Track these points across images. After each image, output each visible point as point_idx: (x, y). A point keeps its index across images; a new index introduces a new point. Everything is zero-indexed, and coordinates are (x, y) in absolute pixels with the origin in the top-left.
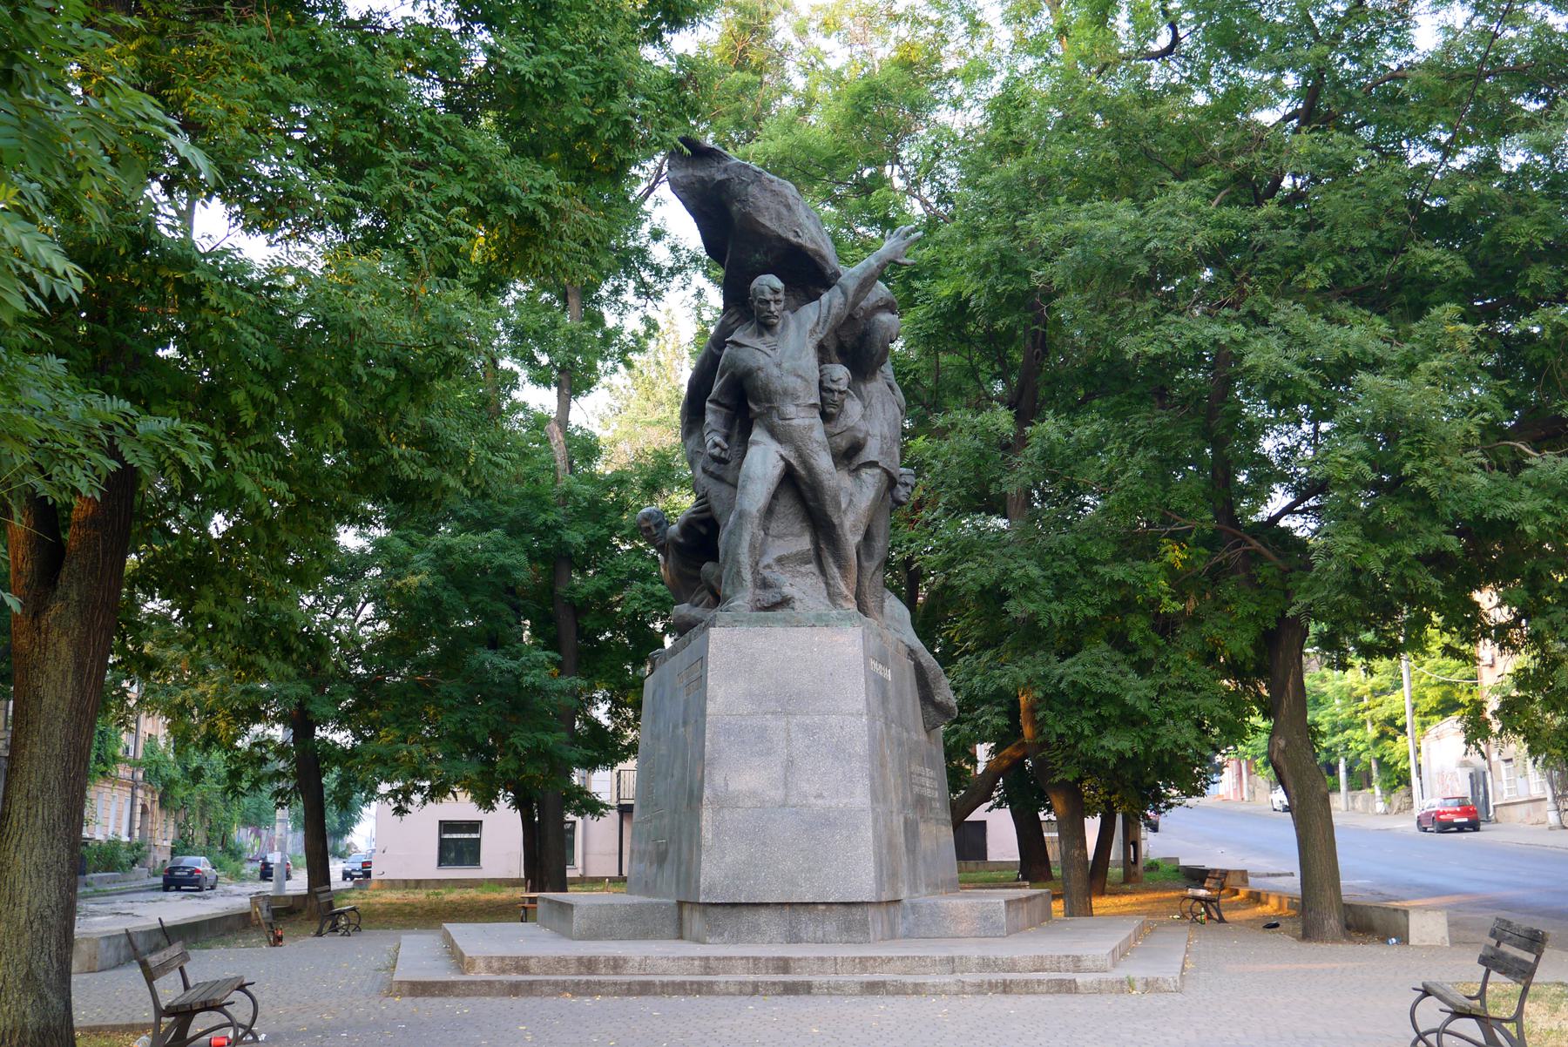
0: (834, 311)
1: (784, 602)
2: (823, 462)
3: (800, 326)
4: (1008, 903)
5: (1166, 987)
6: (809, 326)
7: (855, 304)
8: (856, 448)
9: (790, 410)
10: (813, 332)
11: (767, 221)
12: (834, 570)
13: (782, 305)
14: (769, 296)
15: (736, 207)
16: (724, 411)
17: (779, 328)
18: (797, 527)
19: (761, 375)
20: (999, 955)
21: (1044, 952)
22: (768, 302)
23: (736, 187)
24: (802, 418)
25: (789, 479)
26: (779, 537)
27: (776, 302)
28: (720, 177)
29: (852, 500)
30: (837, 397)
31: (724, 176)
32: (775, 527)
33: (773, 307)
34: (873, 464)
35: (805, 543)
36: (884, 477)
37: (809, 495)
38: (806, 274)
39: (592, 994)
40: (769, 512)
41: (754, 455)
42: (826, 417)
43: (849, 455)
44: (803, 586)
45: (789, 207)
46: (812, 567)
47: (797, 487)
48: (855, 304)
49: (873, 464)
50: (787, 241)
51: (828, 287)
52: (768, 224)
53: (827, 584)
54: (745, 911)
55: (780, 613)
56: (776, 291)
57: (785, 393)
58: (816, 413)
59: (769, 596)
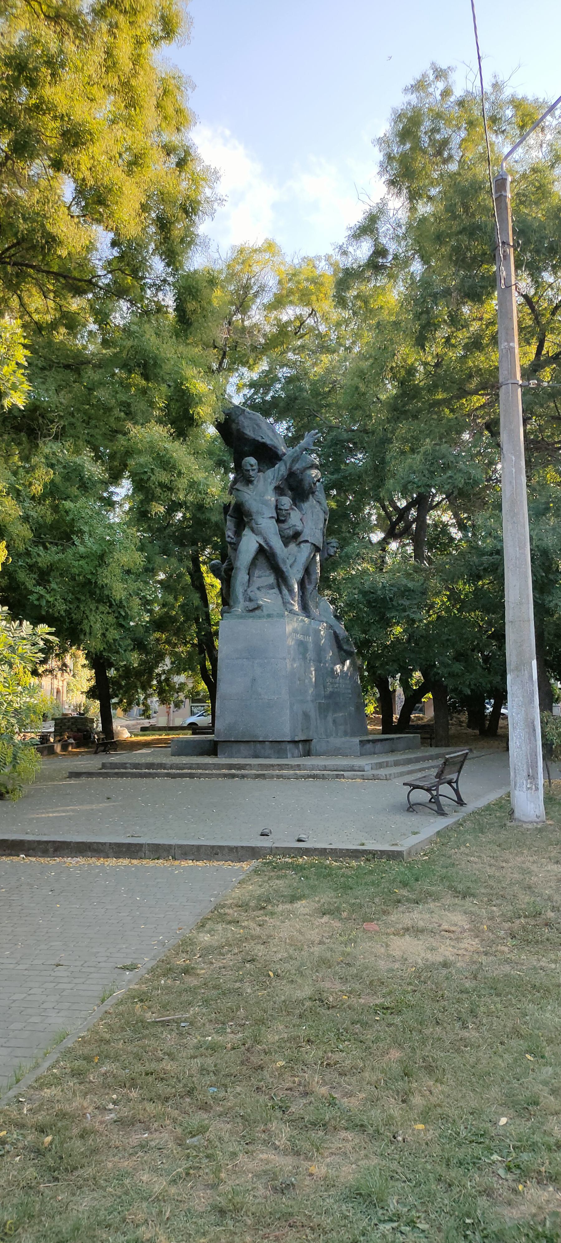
0: (281, 473)
1: (259, 607)
2: (277, 544)
3: (265, 480)
6: (269, 480)
7: (290, 469)
8: (297, 535)
11: (249, 432)
12: (285, 591)
14: (249, 468)
17: (255, 482)
18: (268, 572)
25: (261, 550)
26: (259, 577)
27: (253, 470)
29: (295, 559)
30: (284, 512)
32: (257, 573)
33: (251, 473)
34: (307, 541)
35: (271, 579)
38: (267, 455)
39: (122, 777)
40: (253, 563)
41: (244, 540)
42: (278, 521)
43: (293, 538)
44: (268, 599)
45: (258, 425)
46: (276, 590)
47: (265, 554)
49: (307, 541)
50: (258, 441)
52: (248, 433)
53: (283, 598)
54: (235, 745)
55: (257, 612)
56: (252, 466)
57: (258, 513)
58: (274, 521)
59: (251, 606)
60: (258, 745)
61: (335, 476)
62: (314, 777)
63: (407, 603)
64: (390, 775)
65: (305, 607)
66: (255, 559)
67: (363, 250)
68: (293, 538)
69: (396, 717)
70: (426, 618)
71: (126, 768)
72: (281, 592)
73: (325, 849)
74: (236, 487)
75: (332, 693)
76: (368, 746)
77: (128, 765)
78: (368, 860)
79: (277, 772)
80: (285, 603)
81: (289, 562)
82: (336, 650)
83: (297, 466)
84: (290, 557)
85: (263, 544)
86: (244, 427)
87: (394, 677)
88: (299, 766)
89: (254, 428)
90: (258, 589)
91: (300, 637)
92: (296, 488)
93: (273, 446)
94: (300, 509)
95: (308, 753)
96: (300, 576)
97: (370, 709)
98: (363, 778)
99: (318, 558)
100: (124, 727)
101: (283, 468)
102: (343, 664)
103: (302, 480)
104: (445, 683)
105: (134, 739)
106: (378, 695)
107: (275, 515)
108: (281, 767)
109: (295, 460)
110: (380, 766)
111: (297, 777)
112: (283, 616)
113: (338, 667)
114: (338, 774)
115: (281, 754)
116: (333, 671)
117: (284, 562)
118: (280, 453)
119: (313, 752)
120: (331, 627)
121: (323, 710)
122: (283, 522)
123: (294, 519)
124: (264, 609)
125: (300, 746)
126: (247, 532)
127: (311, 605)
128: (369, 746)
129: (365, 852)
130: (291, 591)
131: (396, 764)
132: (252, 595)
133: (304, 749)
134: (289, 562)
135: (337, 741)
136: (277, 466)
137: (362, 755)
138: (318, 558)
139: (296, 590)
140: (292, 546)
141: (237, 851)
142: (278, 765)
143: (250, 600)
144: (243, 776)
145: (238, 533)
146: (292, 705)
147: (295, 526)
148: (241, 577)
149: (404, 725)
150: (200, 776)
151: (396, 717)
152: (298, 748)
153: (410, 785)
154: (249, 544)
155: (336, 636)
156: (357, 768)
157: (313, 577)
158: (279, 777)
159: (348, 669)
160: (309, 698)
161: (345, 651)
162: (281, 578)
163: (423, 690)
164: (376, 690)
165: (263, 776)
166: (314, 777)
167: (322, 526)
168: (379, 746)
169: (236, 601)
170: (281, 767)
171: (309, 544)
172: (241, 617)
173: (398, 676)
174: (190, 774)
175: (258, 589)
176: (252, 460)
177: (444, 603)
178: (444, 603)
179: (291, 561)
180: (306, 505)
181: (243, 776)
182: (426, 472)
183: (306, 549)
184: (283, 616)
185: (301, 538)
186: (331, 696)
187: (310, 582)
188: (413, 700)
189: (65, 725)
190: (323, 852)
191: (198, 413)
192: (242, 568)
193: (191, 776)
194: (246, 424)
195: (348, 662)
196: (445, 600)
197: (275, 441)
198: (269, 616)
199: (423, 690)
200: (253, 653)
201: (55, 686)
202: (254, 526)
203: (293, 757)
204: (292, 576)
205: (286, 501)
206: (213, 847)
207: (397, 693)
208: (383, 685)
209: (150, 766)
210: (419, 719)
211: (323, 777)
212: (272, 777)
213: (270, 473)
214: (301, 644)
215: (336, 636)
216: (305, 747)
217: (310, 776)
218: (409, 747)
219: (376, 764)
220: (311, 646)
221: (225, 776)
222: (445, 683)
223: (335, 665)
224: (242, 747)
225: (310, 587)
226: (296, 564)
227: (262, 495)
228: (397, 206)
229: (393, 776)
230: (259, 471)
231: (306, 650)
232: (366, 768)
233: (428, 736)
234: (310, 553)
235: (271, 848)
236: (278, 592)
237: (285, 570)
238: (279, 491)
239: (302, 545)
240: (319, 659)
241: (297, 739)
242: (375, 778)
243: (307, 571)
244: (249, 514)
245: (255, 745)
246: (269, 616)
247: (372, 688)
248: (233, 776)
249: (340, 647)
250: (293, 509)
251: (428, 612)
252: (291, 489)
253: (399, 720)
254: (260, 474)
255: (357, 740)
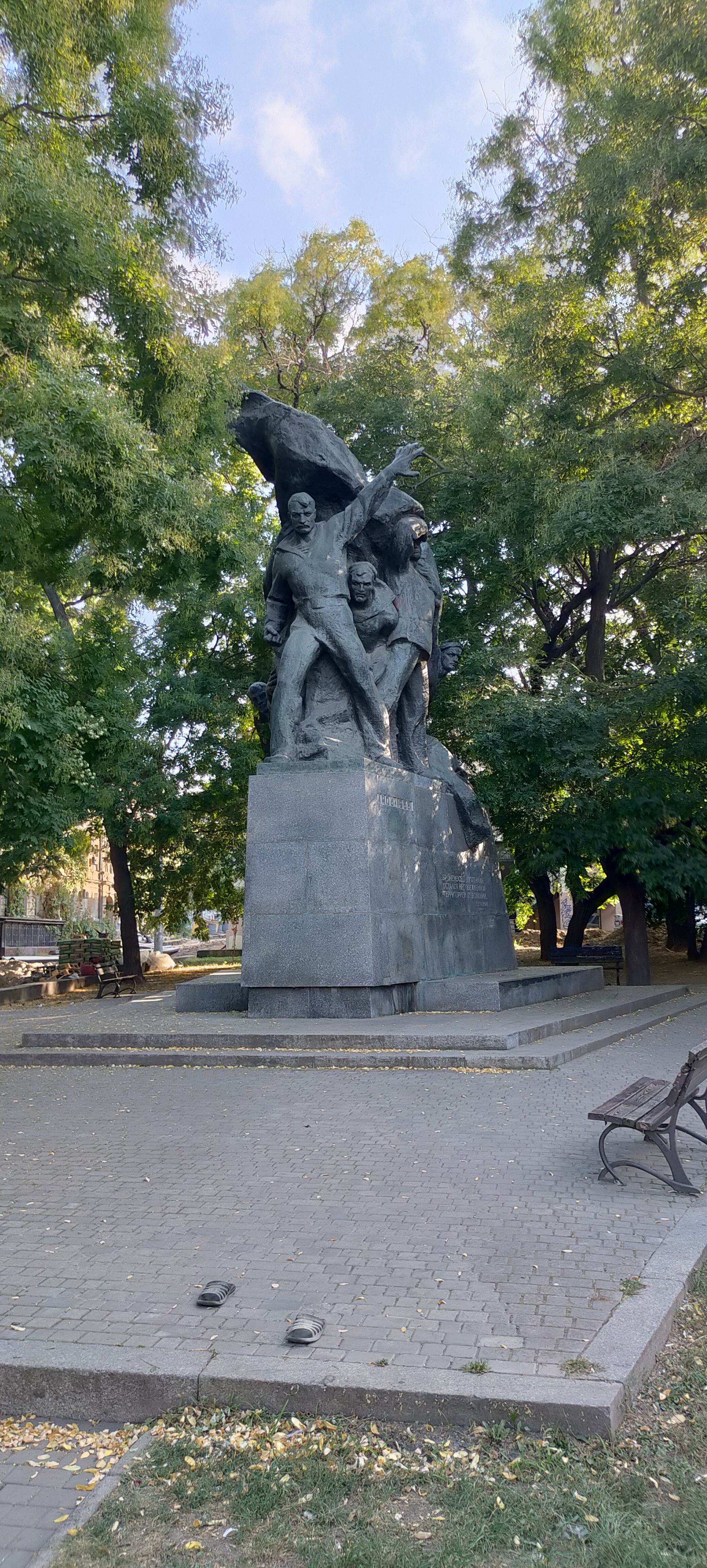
1: (320, 753)
3: (328, 532)
4: (505, 986)
5: (539, 1065)
6: (336, 532)
7: (372, 512)
8: (387, 628)
9: (321, 602)
10: (339, 536)
11: (298, 449)
12: (368, 726)
13: (313, 516)
15: (273, 440)
16: (280, 604)
17: (311, 536)
18: (336, 694)
19: (297, 573)
20: (419, 1034)
21: (434, 1034)
22: (299, 515)
23: (271, 423)
24: (333, 608)
27: (306, 514)
28: (260, 416)
29: (384, 672)
30: (362, 588)
31: (264, 415)
32: (318, 694)
33: (304, 519)
34: (404, 640)
35: (343, 705)
36: (414, 650)
37: (341, 667)
38: (333, 491)
43: (381, 634)
44: (338, 739)
45: (315, 437)
46: (351, 724)
47: (329, 660)
48: (372, 512)
49: (404, 640)
50: (315, 464)
51: (353, 499)
52: (298, 451)
55: (316, 761)
56: (304, 506)
57: (316, 587)
58: (344, 602)
59: (307, 749)
60: (318, 994)
61: (455, 543)
62: (409, 1062)
63: (577, 749)
64: (556, 1058)
65: (404, 755)
66: (313, 668)
67: (497, 183)
68: (381, 634)
69: (562, 931)
70: (608, 772)
71: (64, 1045)
72: (360, 728)
73: (360, 1392)
74: (280, 546)
75: (452, 900)
76: (516, 992)
77: (69, 1039)
78: (492, 1441)
79: (340, 1053)
80: (368, 747)
81: (373, 676)
82: (459, 827)
83: (383, 510)
84: (376, 667)
85: (327, 643)
86: (288, 439)
87: (555, 872)
88: (381, 1039)
89: (306, 441)
90: (321, 721)
91: (394, 803)
92: (382, 547)
93: (341, 472)
94: (393, 587)
95: (409, 1006)
96: (393, 699)
97: (522, 919)
98: (503, 1065)
99: (425, 672)
100: (162, 952)
101: (358, 510)
102: (473, 849)
103: (394, 535)
104: (641, 879)
105: (181, 969)
106: (535, 902)
107: (347, 592)
108: (349, 1041)
109: (380, 494)
110: (536, 1035)
111: (375, 1063)
112: (359, 764)
113: (464, 857)
114: (451, 1057)
115: (359, 1011)
116: (454, 861)
117: (364, 673)
118: (354, 486)
119: (419, 1003)
120: (449, 787)
121: (435, 928)
122: (363, 605)
123: (382, 600)
124: (330, 754)
125: (395, 993)
126: (299, 622)
127: (415, 751)
128: (515, 991)
129: (483, 1409)
130: (376, 722)
131: (566, 1027)
132: (308, 731)
133: (402, 1001)
134: (373, 676)
135: (460, 984)
136: (348, 508)
137: (504, 1007)
138: (425, 672)
139: (387, 722)
140: (380, 650)
141: (97, 1389)
142: (344, 1038)
143: (306, 740)
144: (273, 1062)
145: (285, 627)
146: (377, 922)
147: (382, 613)
148: (289, 699)
149: (575, 950)
150: (193, 1061)
151: (562, 931)
152: (391, 1000)
153: (606, 1118)
154: (302, 643)
155: (458, 801)
156: (492, 1044)
157: (418, 703)
158: (340, 1062)
159: (482, 857)
160: (410, 908)
161: (476, 829)
162: (360, 703)
163: (603, 891)
164: (531, 894)
165: (309, 1062)
166: (409, 1062)
167: (430, 614)
168: (534, 990)
169: (281, 742)
170: (349, 1041)
171: (408, 646)
172: (288, 768)
173: (563, 870)
174: (176, 1056)
175: (321, 721)
176: (305, 497)
177: (637, 747)
178: (637, 747)
179: (378, 674)
180: (402, 580)
181: (273, 1062)
182: (607, 508)
183: (403, 656)
184: (359, 764)
185: (396, 635)
186: (451, 904)
187: (412, 713)
188: (587, 907)
189: (74, 952)
190: (352, 1406)
191: (164, 350)
192: (289, 682)
193: (177, 1061)
194: (292, 435)
195: (481, 846)
196: (641, 742)
197: (347, 465)
198: (336, 765)
199: (603, 891)
200: (307, 830)
201: (105, 894)
202: (311, 611)
203: (380, 1015)
204: (379, 699)
205: (367, 569)
206: (28, 1373)
207: (561, 898)
208: (541, 886)
209: (109, 1040)
210: (597, 935)
211: (426, 1064)
212: (328, 1063)
213: (337, 520)
214: (395, 817)
215: (458, 801)
216: (405, 996)
217: (399, 1062)
218: (587, 988)
219: (529, 1032)
220: (411, 819)
221: (239, 1061)
222: (641, 879)
223: (458, 851)
224: (290, 998)
225: (412, 721)
226: (386, 680)
227: (326, 560)
228: (547, 106)
229: (561, 1060)
230: (318, 519)
231: (404, 824)
232: (510, 1043)
233: (613, 965)
234: (411, 661)
235: (198, 1382)
236: (356, 728)
237: (365, 687)
238: (352, 550)
239: (397, 647)
240: (428, 841)
241: (387, 982)
242: (526, 1065)
243: (407, 691)
244: (302, 592)
245: (315, 996)
246: (336, 765)
247: (525, 892)
248: (255, 1061)
249: (465, 822)
250: (379, 585)
251: (612, 763)
252: (375, 549)
253: (567, 937)
254: (321, 524)
255: (494, 982)
